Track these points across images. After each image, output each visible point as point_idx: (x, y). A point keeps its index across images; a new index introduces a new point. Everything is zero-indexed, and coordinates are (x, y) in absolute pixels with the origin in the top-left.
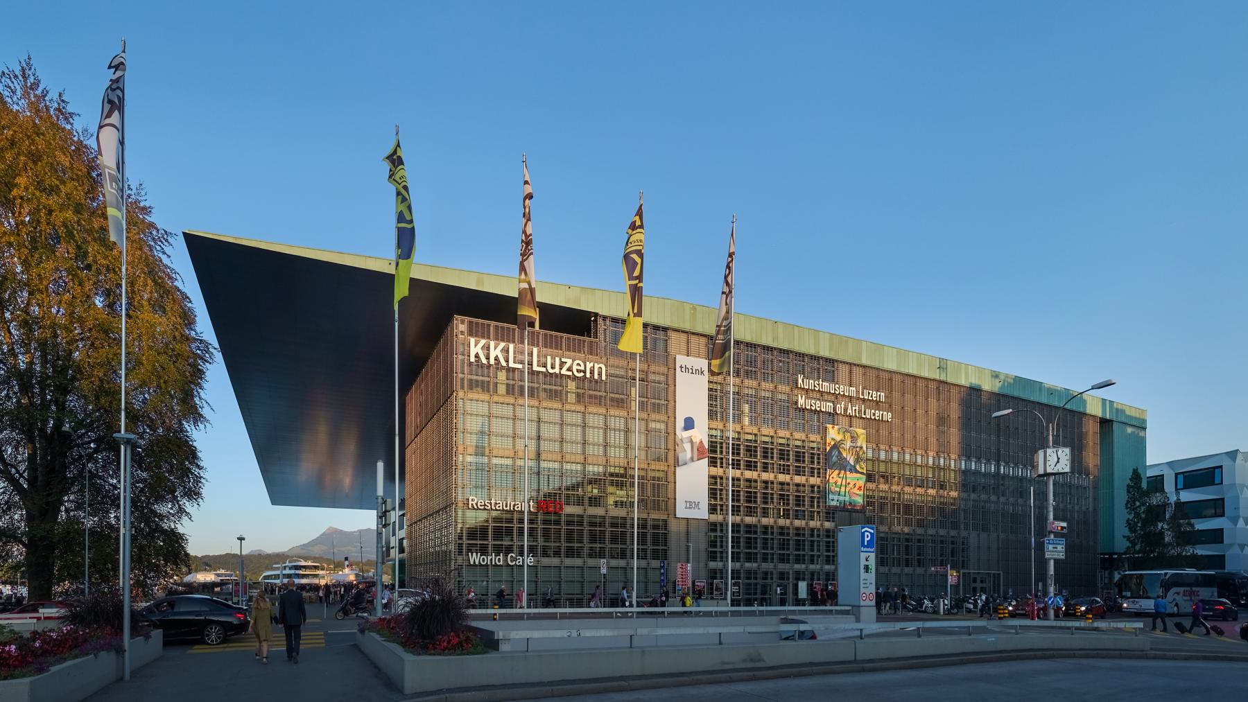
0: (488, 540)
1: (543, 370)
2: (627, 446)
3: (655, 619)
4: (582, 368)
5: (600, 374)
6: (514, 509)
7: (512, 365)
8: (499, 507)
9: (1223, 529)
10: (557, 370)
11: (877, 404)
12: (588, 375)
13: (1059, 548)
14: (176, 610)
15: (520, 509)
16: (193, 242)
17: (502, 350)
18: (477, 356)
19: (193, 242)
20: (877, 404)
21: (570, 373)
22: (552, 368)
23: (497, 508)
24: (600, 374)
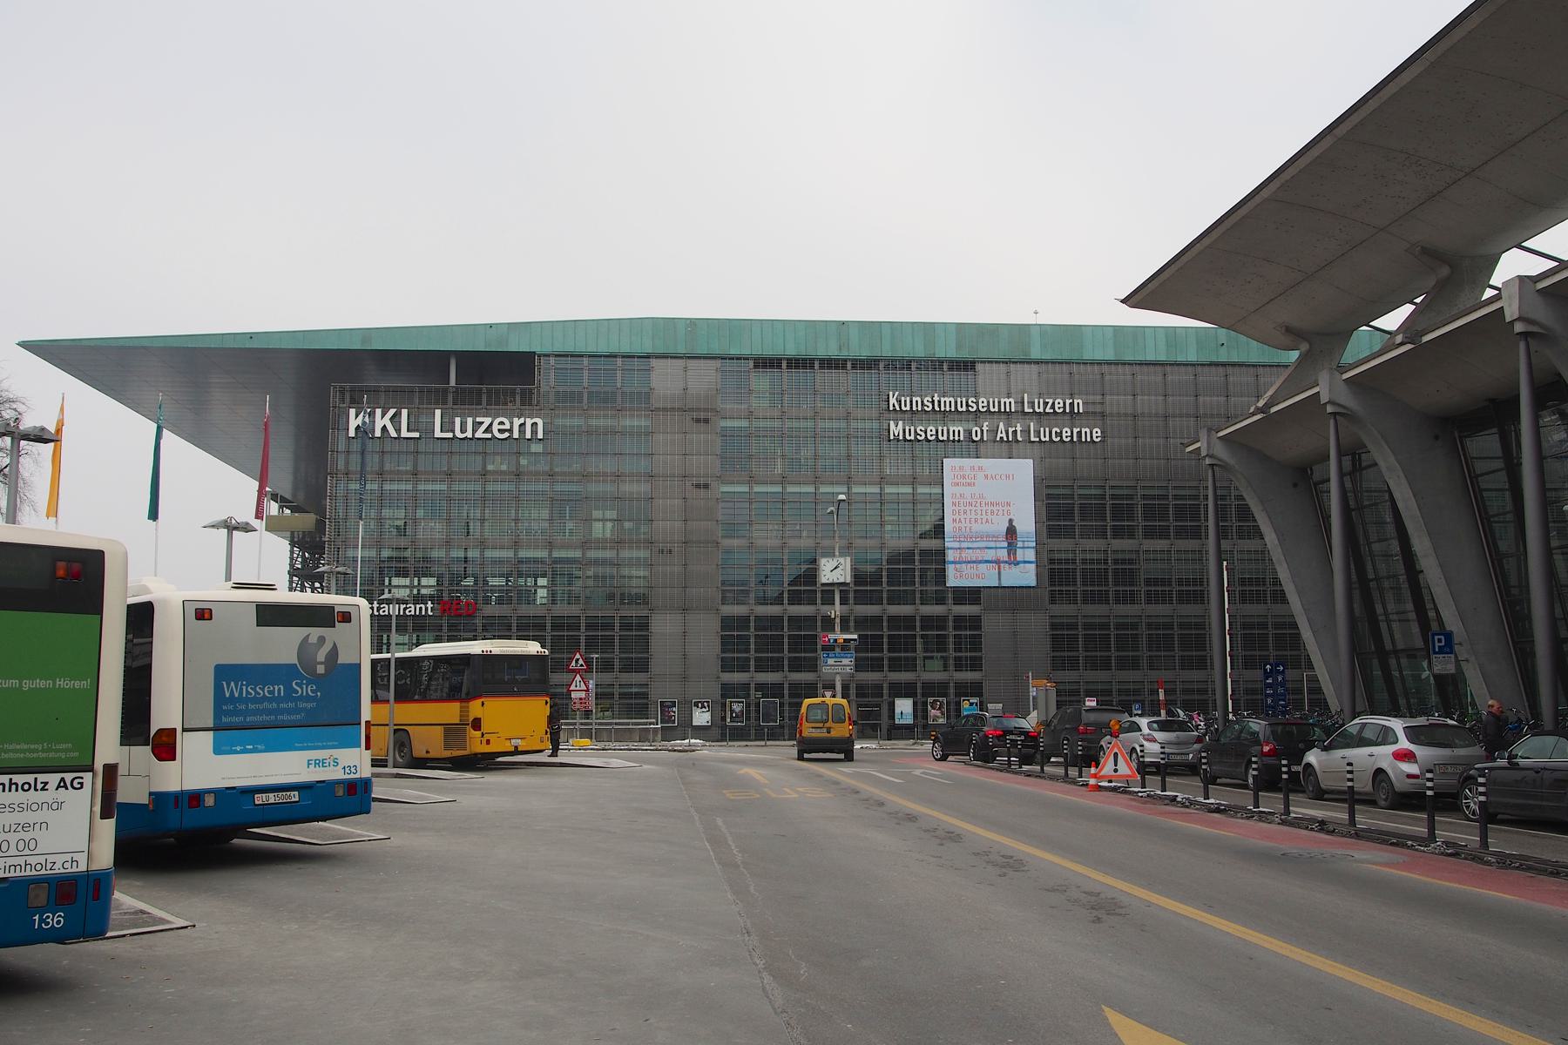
0: (1174, 650)
1: (450, 435)
2: (604, 520)
3: (185, 788)
4: (507, 426)
5: (534, 432)
6: (404, 612)
7: (404, 434)
8: (384, 611)
9: (257, 626)
10: (469, 434)
11: (1072, 416)
12: (516, 435)
13: (846, 661)
14: (561, 758)
15: (386, 613)
16: (1136, 299)
17: (392, 419)
18: (384, 428)
19: (1136, 299)
20: (1072, 416)
21: (489, 436)
22: (462, 432)
23: (382, 613)
24: (534, 432)
